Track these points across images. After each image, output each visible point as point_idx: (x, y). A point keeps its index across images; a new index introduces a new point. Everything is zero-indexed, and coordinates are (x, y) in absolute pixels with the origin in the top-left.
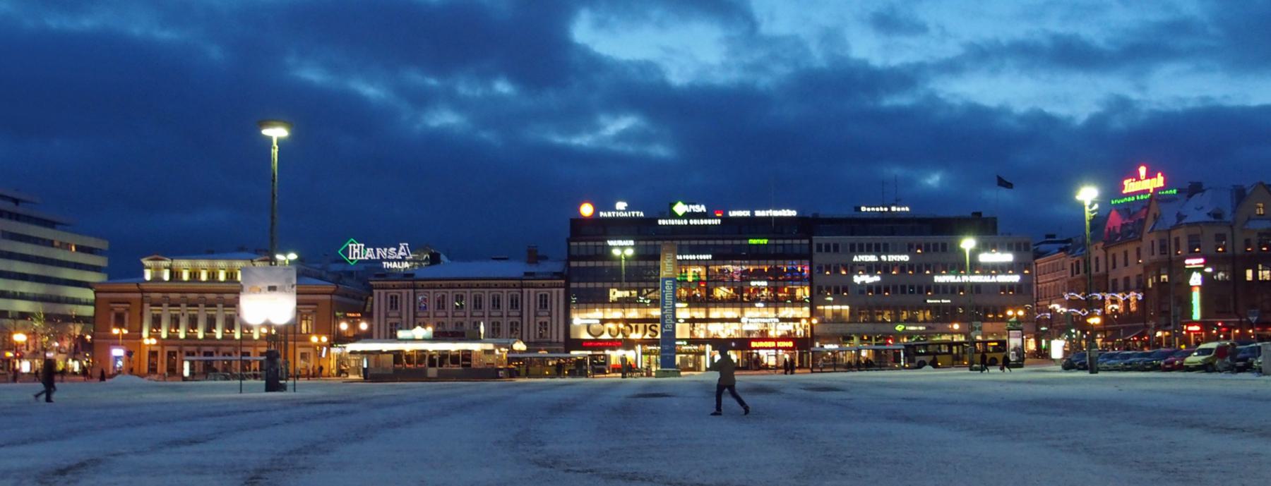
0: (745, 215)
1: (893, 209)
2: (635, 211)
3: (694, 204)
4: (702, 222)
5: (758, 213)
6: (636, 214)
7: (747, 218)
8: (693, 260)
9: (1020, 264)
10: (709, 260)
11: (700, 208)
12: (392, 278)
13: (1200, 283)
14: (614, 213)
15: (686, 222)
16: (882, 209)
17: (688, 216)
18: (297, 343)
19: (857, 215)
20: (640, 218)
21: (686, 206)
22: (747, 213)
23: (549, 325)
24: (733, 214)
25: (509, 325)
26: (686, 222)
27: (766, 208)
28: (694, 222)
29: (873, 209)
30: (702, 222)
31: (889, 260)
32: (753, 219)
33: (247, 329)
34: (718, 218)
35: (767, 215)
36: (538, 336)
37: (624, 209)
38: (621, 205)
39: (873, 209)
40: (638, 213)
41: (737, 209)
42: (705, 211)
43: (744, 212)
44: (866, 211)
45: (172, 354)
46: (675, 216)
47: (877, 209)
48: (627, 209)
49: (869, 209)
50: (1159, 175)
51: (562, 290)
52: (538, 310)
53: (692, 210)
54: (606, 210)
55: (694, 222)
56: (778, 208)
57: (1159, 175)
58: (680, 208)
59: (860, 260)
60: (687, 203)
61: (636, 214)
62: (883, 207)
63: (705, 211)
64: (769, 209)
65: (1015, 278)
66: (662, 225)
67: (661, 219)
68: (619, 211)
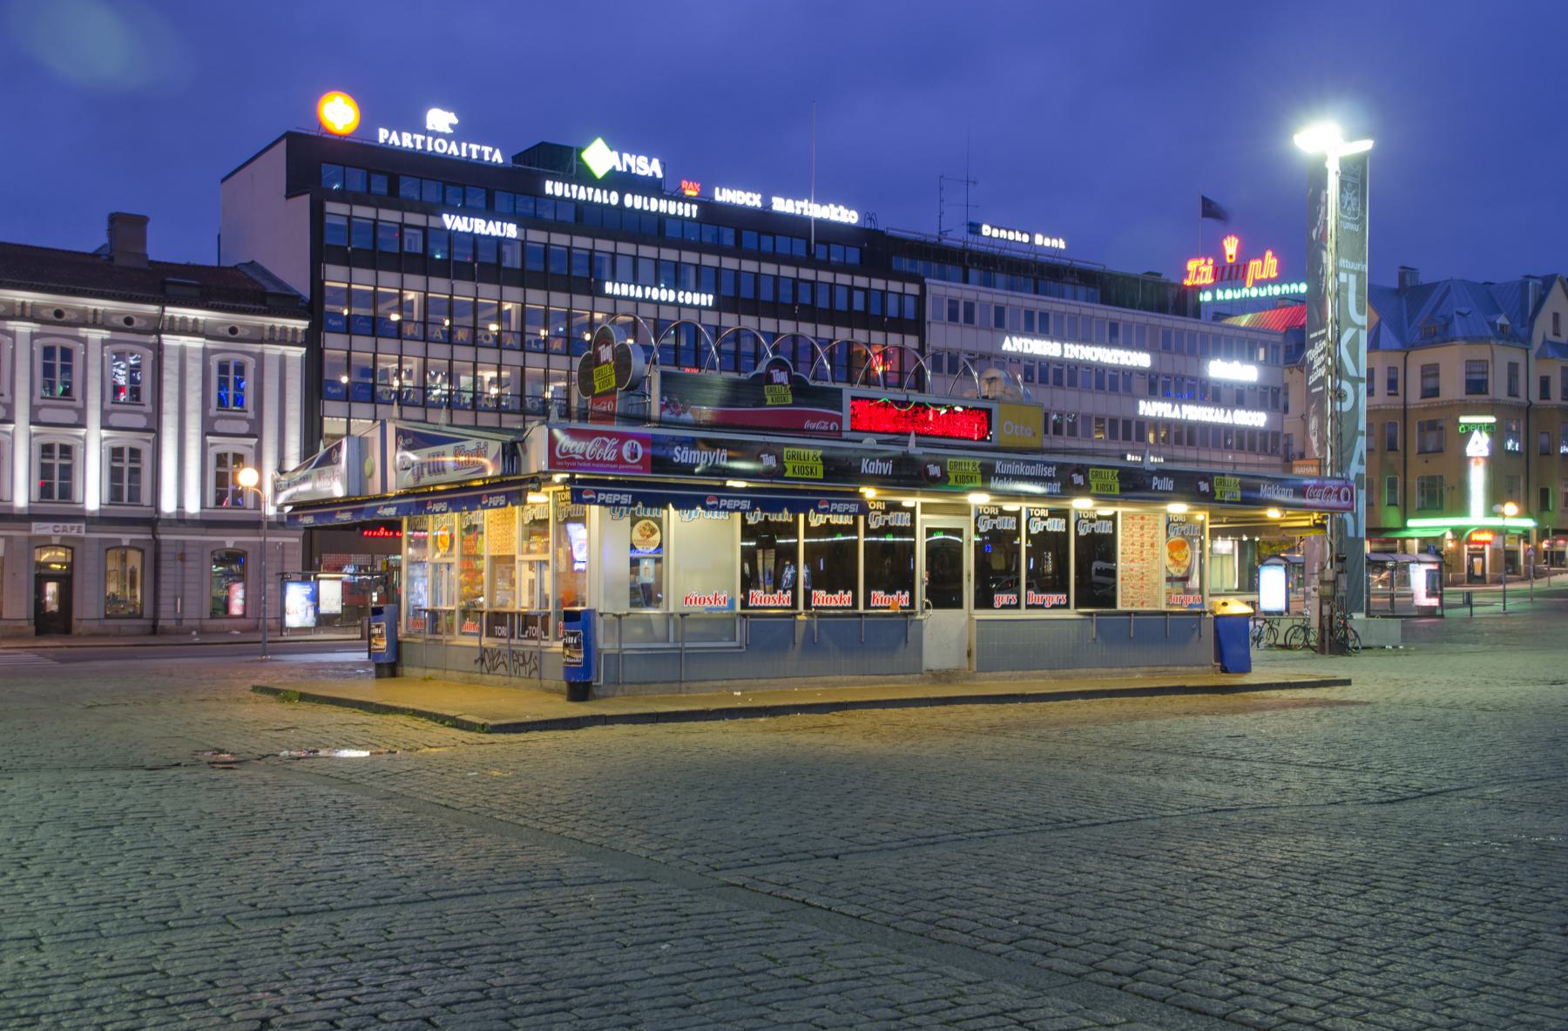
0: (749, 204)
1: (1039, 240)
2: (481, 143)
3: (636, 151)
4: (654, 205)
5: (781, 205)
6: (480, 153)
7: (753, 210)
8: (667, 303)
9: (1266, 388)
10: (706, 308)
11: (648, 167)
12: (783, 244)
13: (1486, 453)
14: (419, 138)
15: (614, 198)
16: (1018, 237)
17: (621, 181)
18: (1501, 609)
19: (973, 243)
20: (492, 168)
21: (615, 154)
22: (752, 200)
23: (146, 458)
24: (726, 196)
25: (37, 452)
26: (614, 198)
27: (797, 195)
28: (633, 201)
29: (1003, 234)
30: (654, 205)
31: (1066, 355)
32: (764, 221)
33: (1205, 480)
34: (691, 200)
35: (798, 212)
36: (211, 502)
37: (449, 131)
38: (440, 119)
39: (1003, 234)
40: (487, 150)
41: (733, 185)
42: (660, 175)
43: (749, 195)
44: (991, 236)
45: (386, 671)
46: (584, 177)
47: (1011, 236)
48: (458, 135)
49: (995, 233)
50: (1269, 254)
51: (296, 353)
52: (213, 412)
53: (629, 168)
54: (398, 126)
55: (633, 201)
56: (822, 200)
57: (1269, 254)
58: (599, 157)
59: (1014, 349)
60: (618, 143)
61: (480, 153)
62: (1022, 233)
63: (660, 175)
64: (802, 199)
65: (1256, 419)
66: (553, 197)
67: (555, 179)
68: (436, 135)
